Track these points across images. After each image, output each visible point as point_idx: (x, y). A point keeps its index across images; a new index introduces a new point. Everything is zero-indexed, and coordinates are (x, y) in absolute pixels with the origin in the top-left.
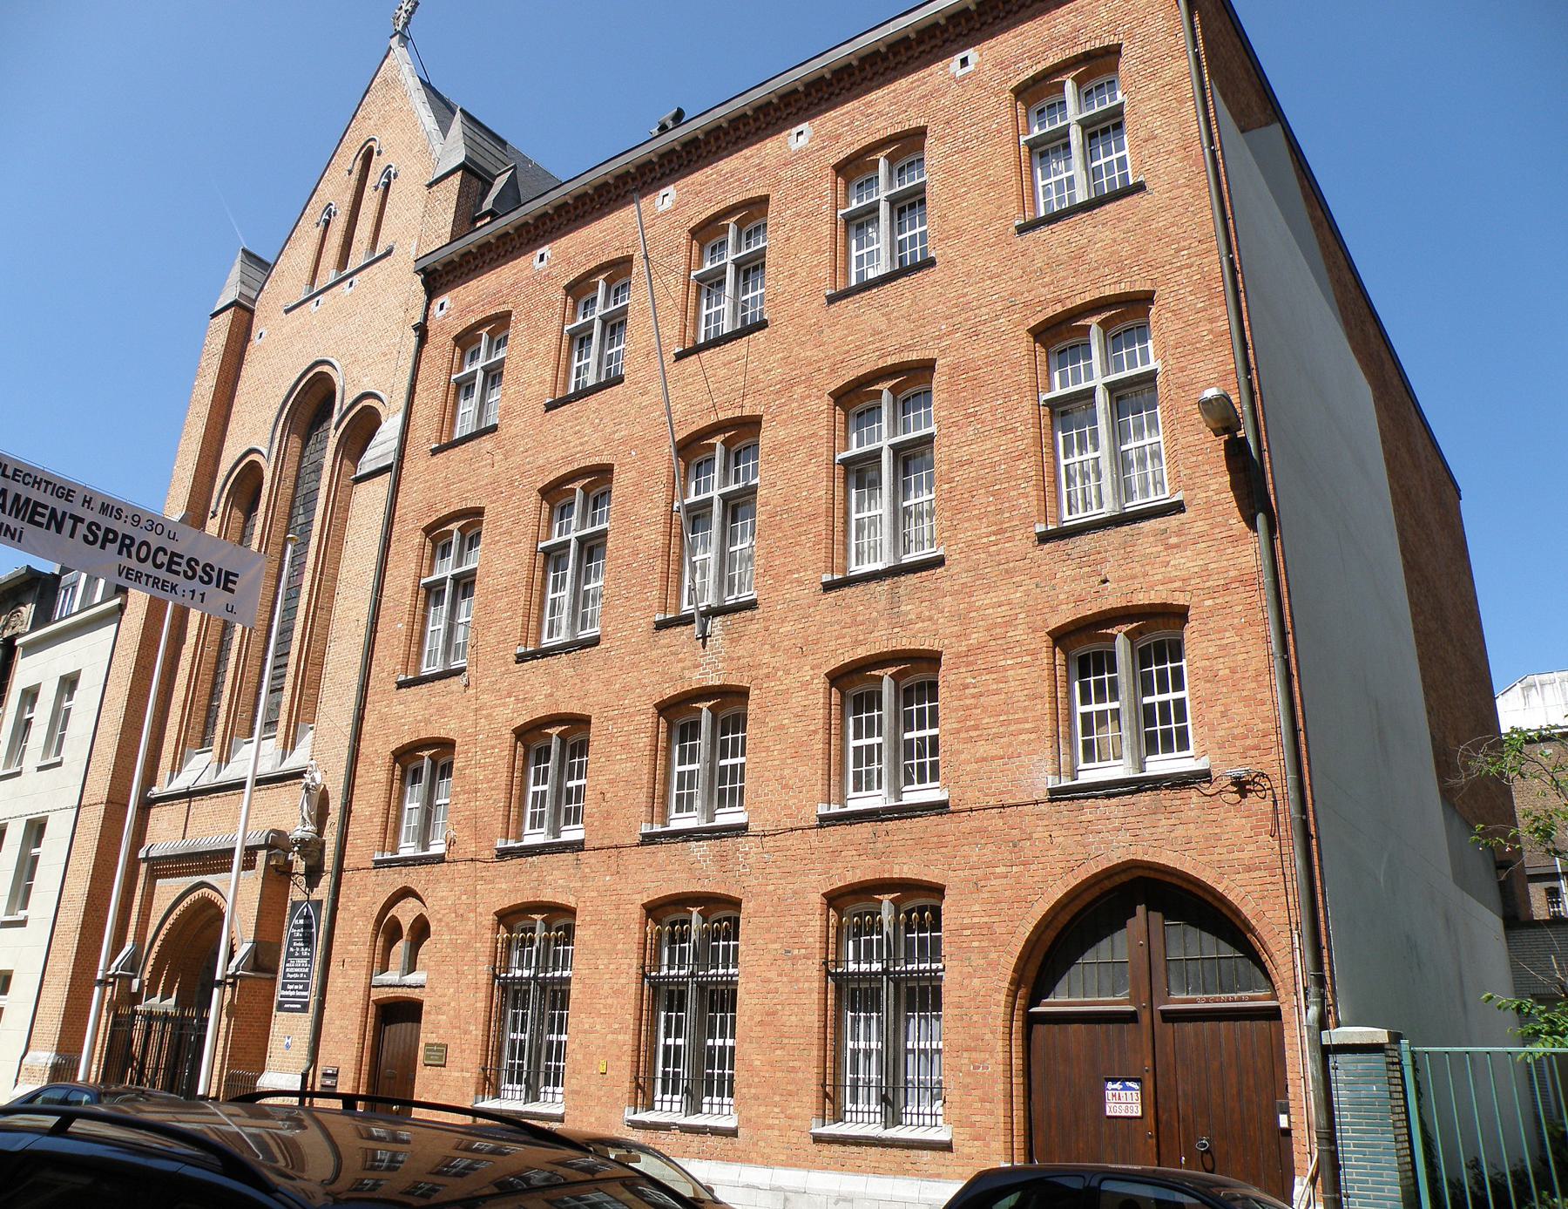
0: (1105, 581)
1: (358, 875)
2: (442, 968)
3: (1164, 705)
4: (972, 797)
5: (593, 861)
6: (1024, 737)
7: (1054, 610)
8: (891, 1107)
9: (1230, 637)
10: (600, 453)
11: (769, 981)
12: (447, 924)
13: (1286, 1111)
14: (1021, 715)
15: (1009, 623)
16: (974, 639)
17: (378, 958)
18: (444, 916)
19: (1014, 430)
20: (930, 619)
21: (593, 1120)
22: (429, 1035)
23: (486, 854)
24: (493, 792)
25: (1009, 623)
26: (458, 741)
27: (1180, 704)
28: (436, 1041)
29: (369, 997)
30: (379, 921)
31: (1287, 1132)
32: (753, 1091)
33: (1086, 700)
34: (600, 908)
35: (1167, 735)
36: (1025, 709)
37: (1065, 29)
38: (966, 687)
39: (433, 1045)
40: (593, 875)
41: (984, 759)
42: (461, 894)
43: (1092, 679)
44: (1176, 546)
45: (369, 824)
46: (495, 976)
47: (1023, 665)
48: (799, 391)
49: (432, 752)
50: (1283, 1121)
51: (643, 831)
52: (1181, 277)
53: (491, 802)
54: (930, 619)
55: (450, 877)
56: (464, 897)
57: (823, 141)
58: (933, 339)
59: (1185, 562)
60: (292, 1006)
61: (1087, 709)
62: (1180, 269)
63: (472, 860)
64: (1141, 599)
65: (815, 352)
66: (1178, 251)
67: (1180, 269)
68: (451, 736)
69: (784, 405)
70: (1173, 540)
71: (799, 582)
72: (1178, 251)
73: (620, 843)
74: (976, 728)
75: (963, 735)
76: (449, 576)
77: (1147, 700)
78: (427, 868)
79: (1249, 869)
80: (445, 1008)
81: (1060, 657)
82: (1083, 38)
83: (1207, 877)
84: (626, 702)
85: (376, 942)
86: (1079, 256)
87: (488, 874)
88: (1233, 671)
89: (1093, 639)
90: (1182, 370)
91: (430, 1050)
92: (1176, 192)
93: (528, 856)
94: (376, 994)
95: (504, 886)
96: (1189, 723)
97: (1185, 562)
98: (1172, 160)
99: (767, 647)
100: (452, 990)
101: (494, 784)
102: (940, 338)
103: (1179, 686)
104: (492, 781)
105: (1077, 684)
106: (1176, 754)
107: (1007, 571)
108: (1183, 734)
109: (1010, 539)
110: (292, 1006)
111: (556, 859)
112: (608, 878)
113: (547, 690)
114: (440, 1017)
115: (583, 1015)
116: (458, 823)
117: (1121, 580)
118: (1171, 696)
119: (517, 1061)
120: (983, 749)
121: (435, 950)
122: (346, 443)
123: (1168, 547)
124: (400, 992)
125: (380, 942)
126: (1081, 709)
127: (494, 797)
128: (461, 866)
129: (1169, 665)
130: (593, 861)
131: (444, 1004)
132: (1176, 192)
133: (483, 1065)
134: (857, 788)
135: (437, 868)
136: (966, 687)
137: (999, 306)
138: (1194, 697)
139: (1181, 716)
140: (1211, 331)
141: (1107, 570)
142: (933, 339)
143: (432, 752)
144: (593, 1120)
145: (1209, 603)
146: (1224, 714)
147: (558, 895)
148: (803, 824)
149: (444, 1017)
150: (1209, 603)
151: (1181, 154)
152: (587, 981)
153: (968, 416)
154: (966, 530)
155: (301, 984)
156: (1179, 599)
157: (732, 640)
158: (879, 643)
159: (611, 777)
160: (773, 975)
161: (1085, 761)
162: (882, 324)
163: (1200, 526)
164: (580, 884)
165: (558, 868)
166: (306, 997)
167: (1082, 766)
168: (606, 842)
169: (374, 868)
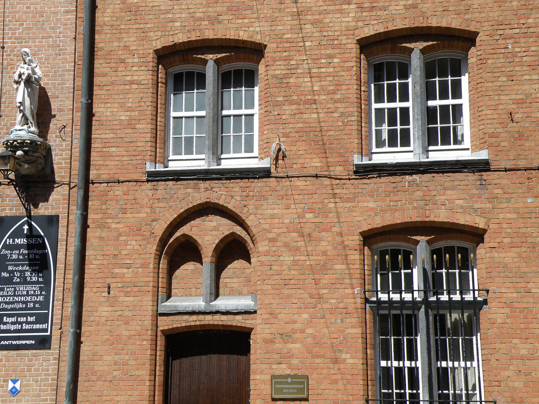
1: (118, 190)
2: (286, 292)
3: (444, 108)
5: (504, 182)
12: (286, 245)
17: (162, 282)
18: (279, 235)
22: (274, 366)
23: (338, 170)
24: (339, 105)
26: (271, 47)
27: (405, 112)
28: (288, 372)
29: (157, 327)
30: (163, 241)
33: (380, 99)
34: (521, 230)
39: (280, 376)
40: (506, 196)
42: (304, 212)
43: (386, 83)
45: (130, 131)
46: (367, 301)
49: (219, 56)
51: (148, 170)
53: (336, 115)
55: (282, 193)
56: (309, 216)
60: (18, 342)
61: (404, 105)
68: (258, 39)
77: (431, 103)
78: (243, 183)
80: (298, 335)
81: (364, 63)
84: (530, 21)
85: (159, 264)
87: (344, 191)
89: (186, 61)
91: (276, 383)
93: (405, 174)
94: (165, 324)
95: (372, 205)
96: (411, 126)
100: (305, 316)
101: (337, 97)
103: (404, 97)
105: (373, 85)
106: (399, 149)
108: (406, 134)
110: (18, 342)
111: (448, 179)
112: (530, 200)
114: (290, 346)
115: (514, 341)
116: (286, 135)
118: (398, 105)
119: (408, 391)
121: (270, 272)
124: (208, 320)
125: (164, 263)
126: (375, 106)
127: (340, 110)
128: (299, 183)
129: (397, 81)
130: (504, 182)
131: (294, 331)
133: (366, 397)
134: (177, 152)
135: (258, 184)
139: (405, 120)
143: (219, 56)
147: (457, 216)
149: (298, 345)
152: (516, 305)
155: (31, 315)
159: (520, 97)
161: (378, 146)
164: (489, 206)
165: (453, 188)
166: (46, 330)
167: (375, 150)
168: (522, 164)
169: (148, 181)
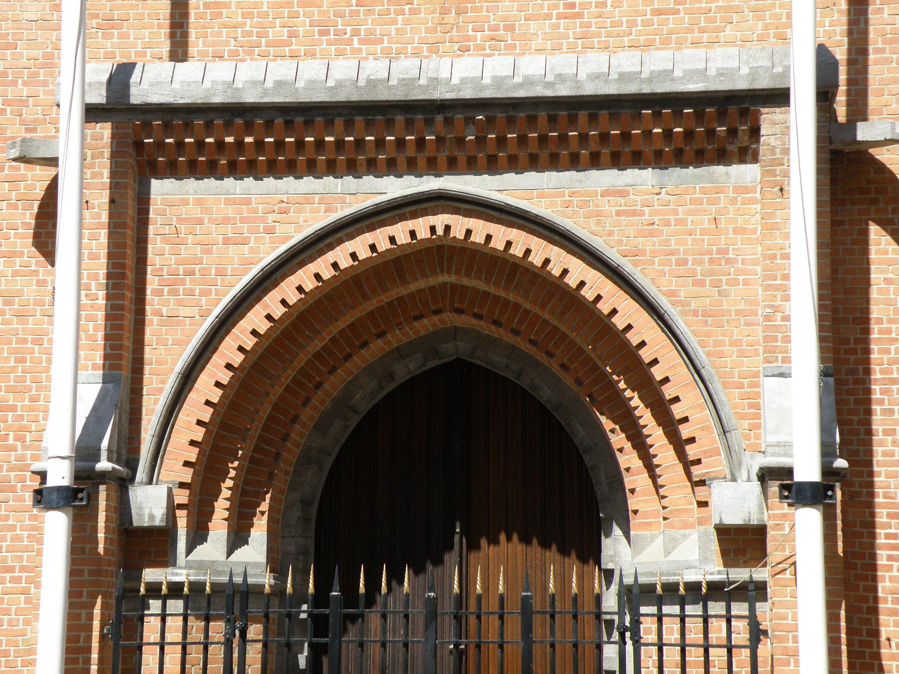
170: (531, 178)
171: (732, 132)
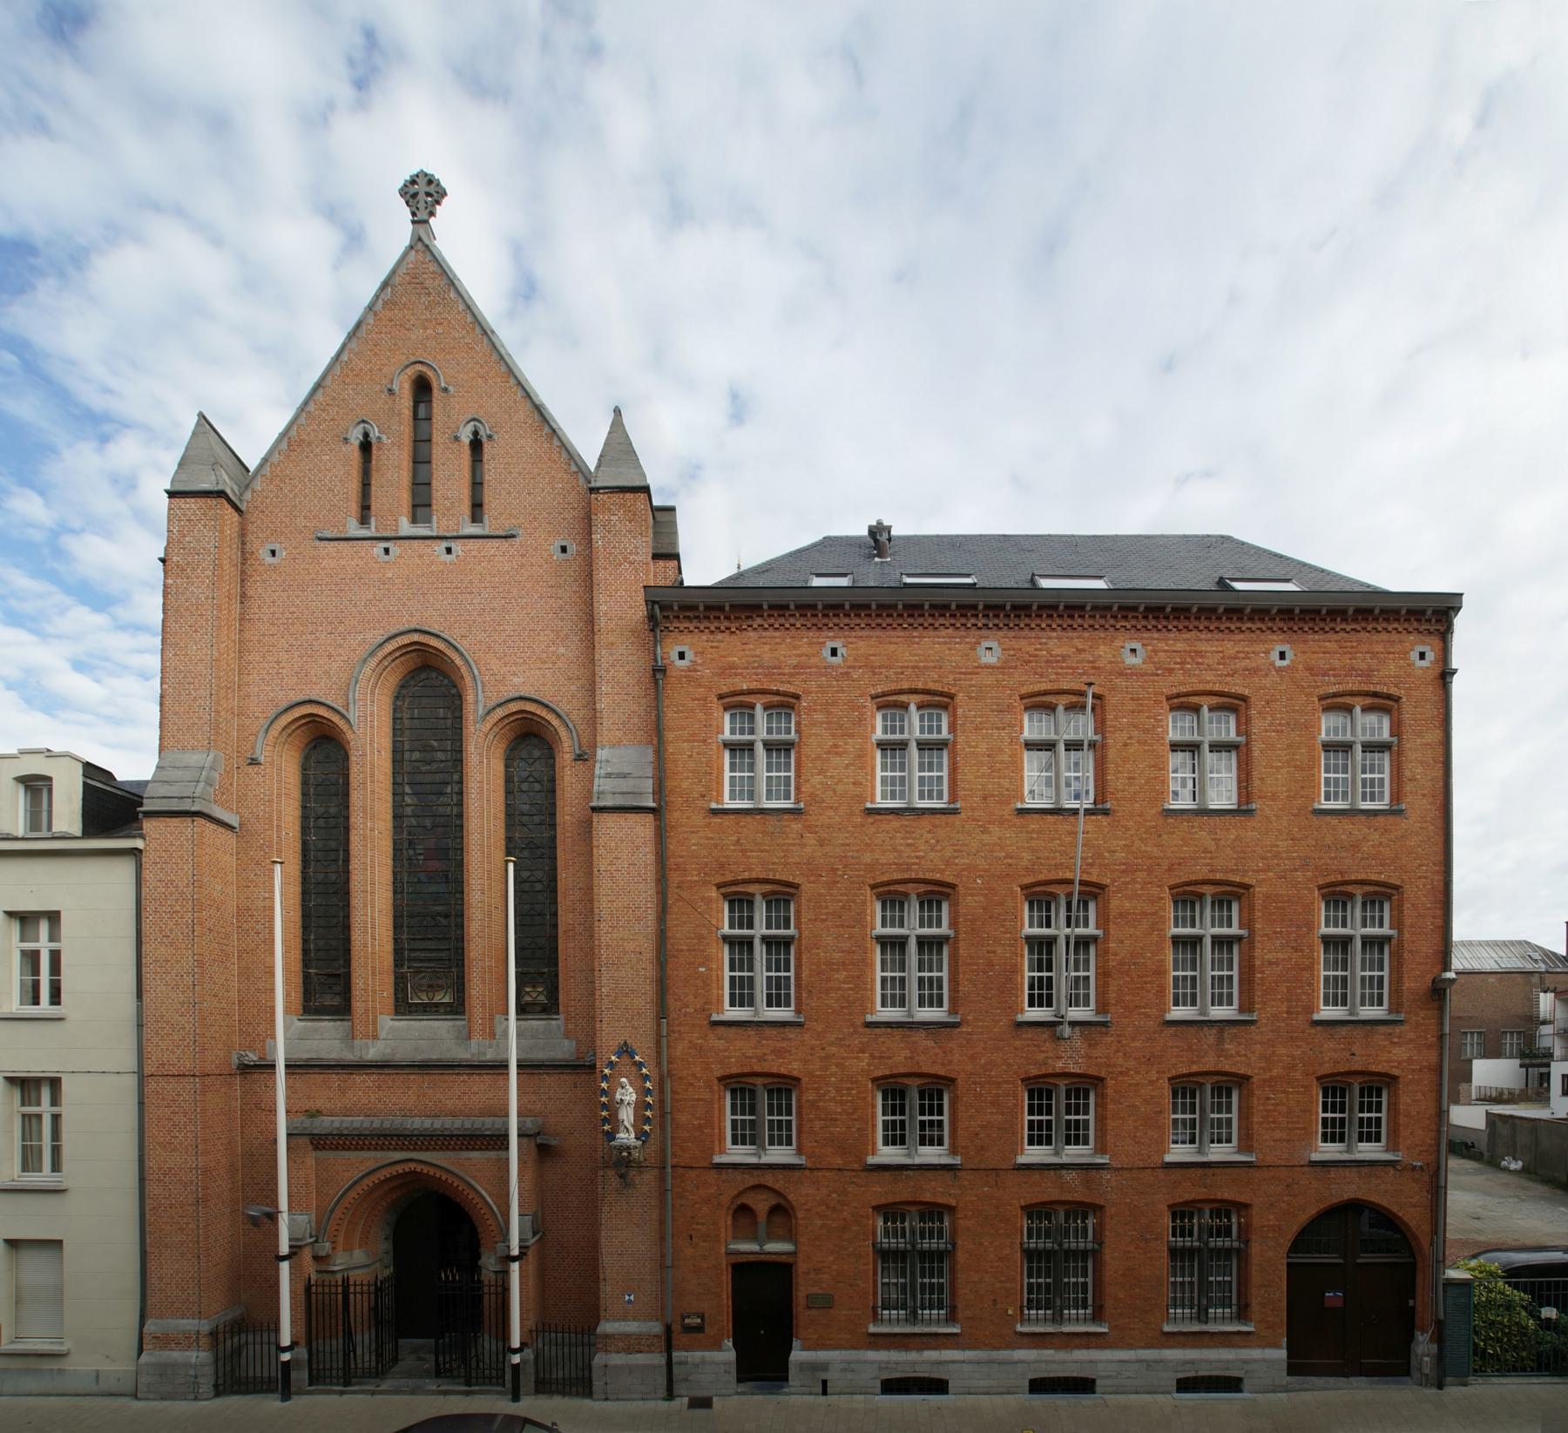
0: (1353, 1054)
4: (1270, 1159)
6: (1298, 1132)
7: (1321, 1065)
8: (1015, 726)
9: (1419, 1096)
10: (942, 872)
11: (1129, 1252)
13: (1414, 1298)
14: (1295, 1119)
15: (1293, 1067)
16: (1274, 1073)
19: (1302, 951)
20: (1245, 1055)
21: (987, 1333)
25: (1293, 1067)
31: (1413, 1308)
32: (1119, 1311)
35: (1369, 1133)
36: (1299, 1117)
37: (1363, 666)
38: (1269, 1099)
41: (1277, 1140)
44: (1395, 1043)
47: (1298, 1093)
48: (1141, 876)
50: (1411, 1303)
52: (1420, 883)
54: (1245, 1055)
56: (834, 1195)
57: (1157, 669)
58: (1253, 871)
59: (1400, 1053)
62: (1420, 877)
63: (839, 1169)
64: (1373, 1068)
65: (1155, 849)
66: (1420, 865)
67: (1420, 877)
69: (1128, 883)
70: (1396, 1040)
71: (1147, 1016)
72: (1420, 865)
73: (996, 1167)
74: (1274, 1122)
75: (1264, 1125)
76: (758, 936)
79: (1415, 1206)
82: (1375, 680)
83: (1394, 1209)
86: (1355, 847)
88: (1418, 1113)
90: (1413, 942)
92: (1425, 825)
97: (1400, 1053)
98: (1424, 801)
99: (1121, 1054)
102: (1258, 871)
104: (852, 1114)
107: (1292, 1037)
109: (1296, 1019)
113: (907, 1053)
117: (1361, 1055)
120: (1278, 1135)
122: (397, 658)
123: (1392, 1043)
132: (1425, 825)
136: (1269, 1099)
137: (1297, 863)
138: (1317, 1113)
140: (1432, 923)
141: (1356, 1048)
142: (1253, 871)
144: (987, 1333)
145: (1410, 1077)
146: (1412, 1133)
148: (1152, 1165)
150: (1410, 1077)
151: (1431, 800)
153: (1275, 932)
154: (1273, 1006)
156: (1395, 1072)
157: (1090, 1045)
158: (1209, 1063)
160: (1132, 1249)
162: (1211, 845)
163: (1411, 1035)
170: (435, 1154)
171: (503, 1144)
